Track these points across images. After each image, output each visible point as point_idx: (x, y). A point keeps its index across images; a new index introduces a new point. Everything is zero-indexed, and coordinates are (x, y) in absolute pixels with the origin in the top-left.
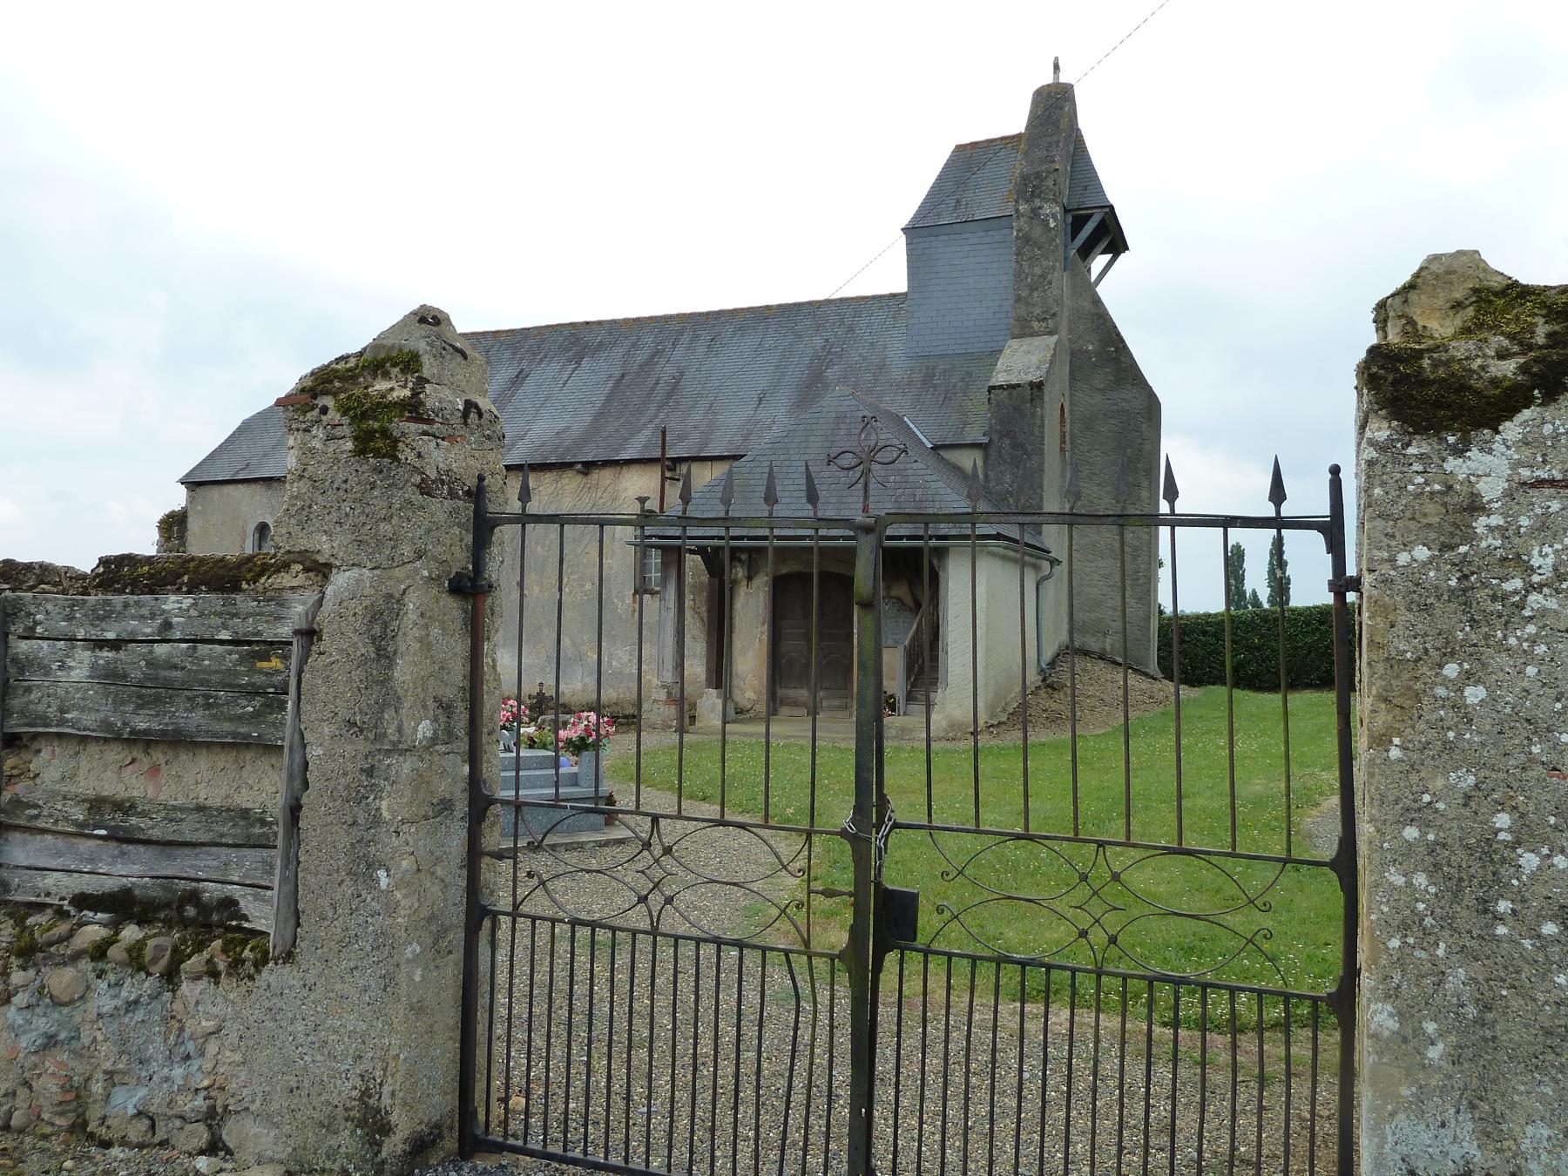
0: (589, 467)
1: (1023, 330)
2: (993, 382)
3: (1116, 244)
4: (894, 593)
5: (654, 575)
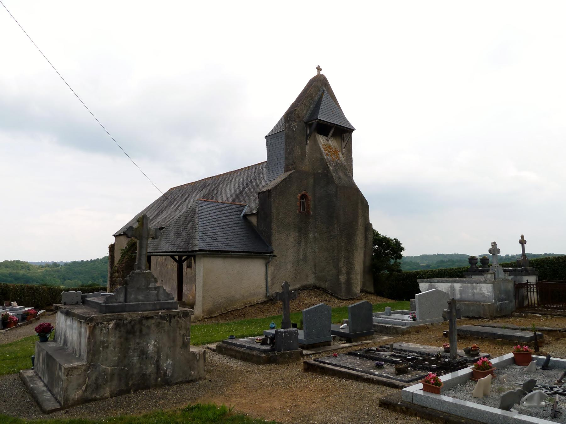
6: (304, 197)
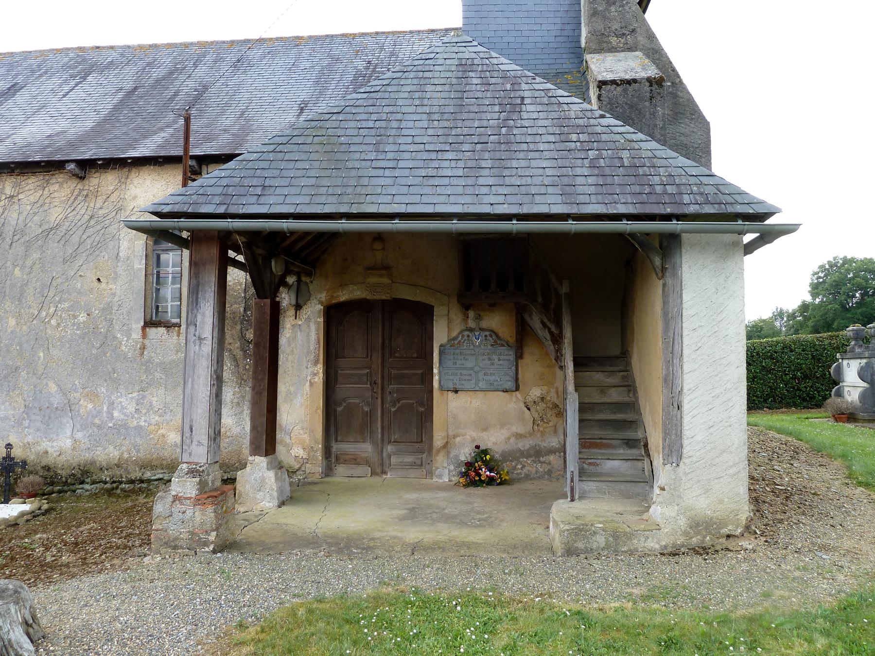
0: (87, 167)
4: (485, 324)
5: (173, 294)
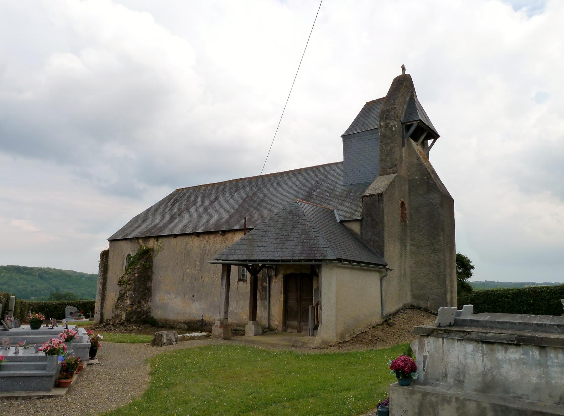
0: (224, 232)
1: (384, 172)
2: (365, 194)
3: (435, 136)
6: (403, 204)
